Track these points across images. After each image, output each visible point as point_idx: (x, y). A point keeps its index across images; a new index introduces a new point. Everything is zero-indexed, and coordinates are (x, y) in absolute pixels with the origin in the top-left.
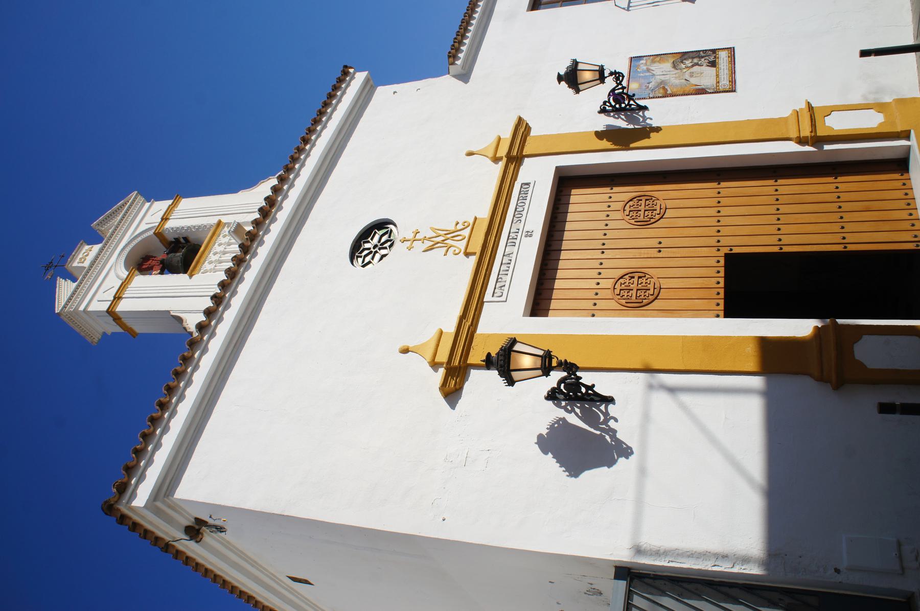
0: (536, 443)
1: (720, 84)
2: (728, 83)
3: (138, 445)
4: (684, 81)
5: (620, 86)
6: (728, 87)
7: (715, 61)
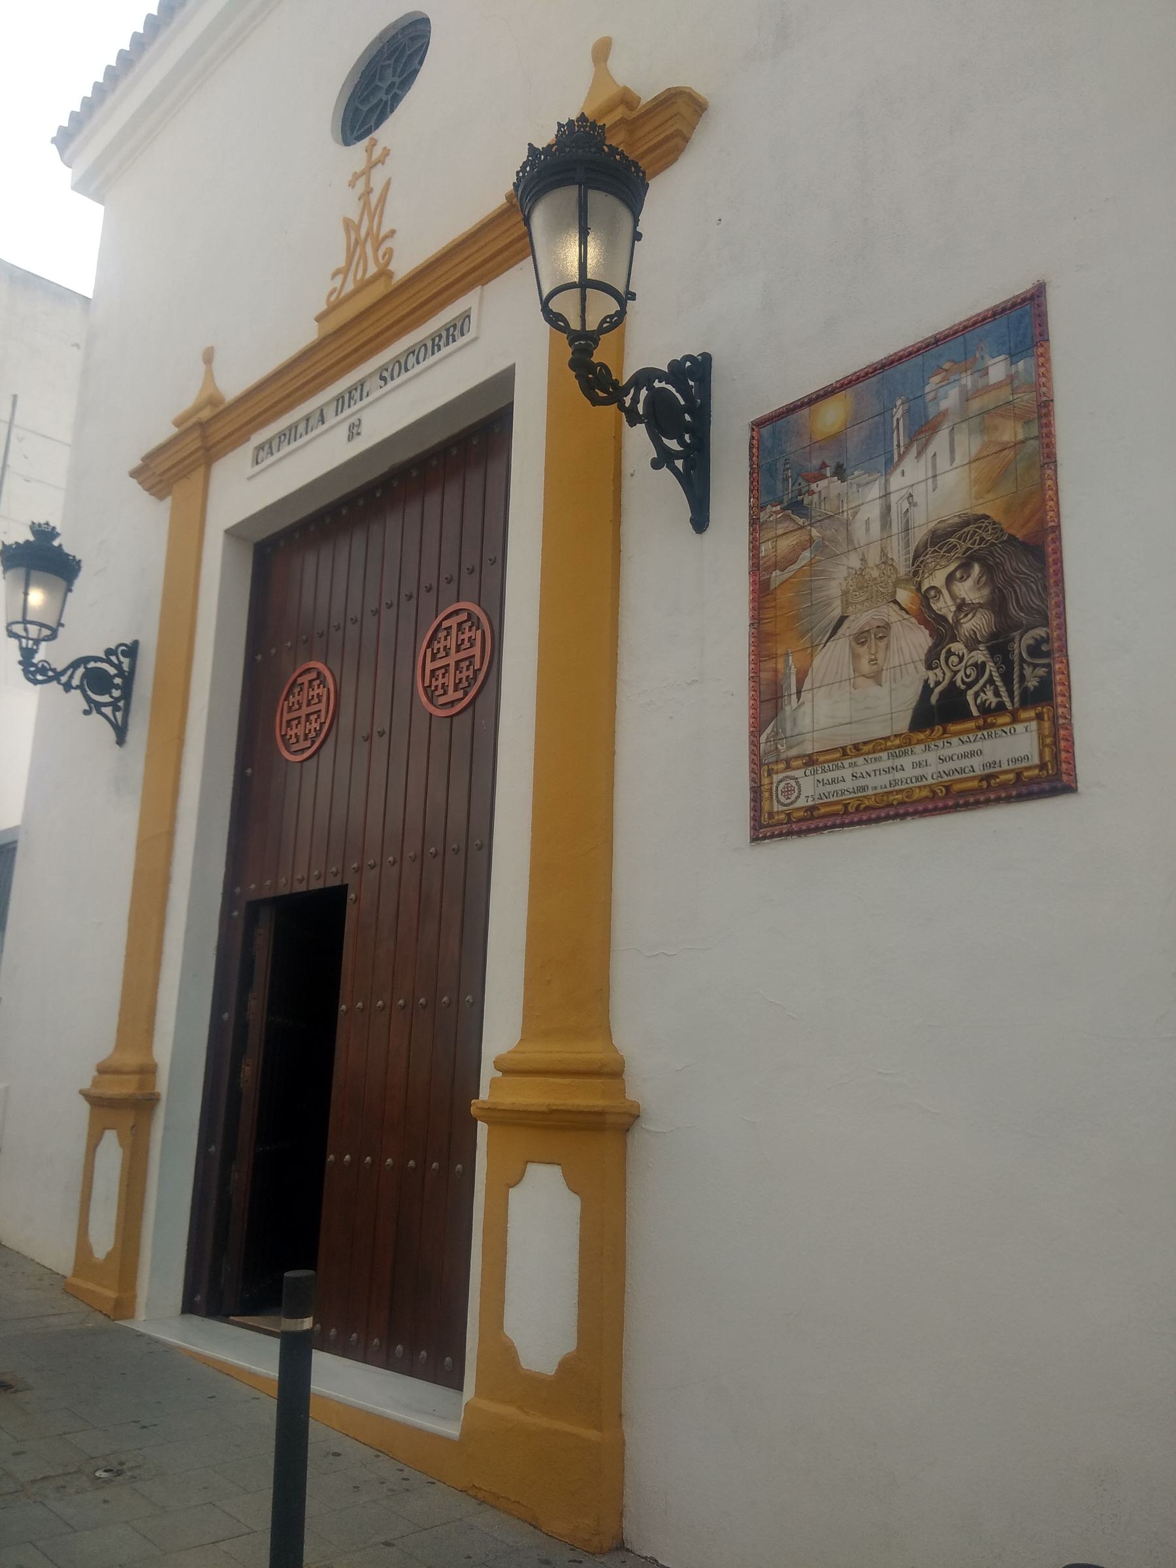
0: (4, 544)
1: (798, 773)
2: (801, 803)
3: (791, 472)
4: (837, 613)
5: (64, 679)
6: (776, 807)
7: (968, 716)
